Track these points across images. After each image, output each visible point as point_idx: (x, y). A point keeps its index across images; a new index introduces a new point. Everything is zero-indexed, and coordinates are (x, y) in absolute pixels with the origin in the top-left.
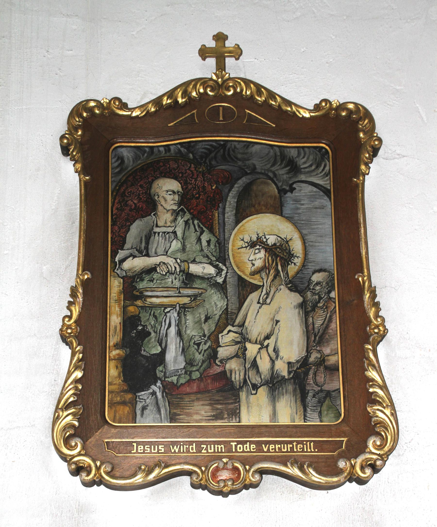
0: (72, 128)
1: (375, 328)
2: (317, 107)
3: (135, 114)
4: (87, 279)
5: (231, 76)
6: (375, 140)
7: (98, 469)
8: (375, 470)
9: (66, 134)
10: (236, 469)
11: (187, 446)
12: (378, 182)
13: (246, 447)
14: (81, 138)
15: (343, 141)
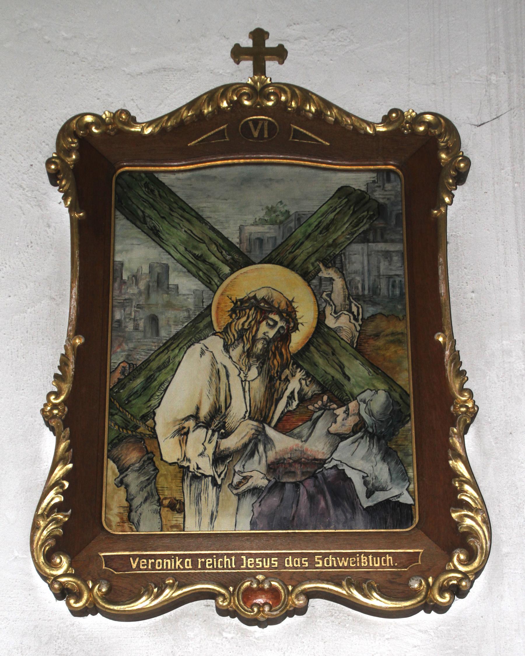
0: (62, 149)
1: (461, 406)
2: (386, 120)
5: (273, 81)
6: (461, 161)
7: (91, 590)
8: (459, 592)
10: (274, 591)
11: (153, 561)
12: (463, 212)
13: (288, 561)
15: (422, 161)
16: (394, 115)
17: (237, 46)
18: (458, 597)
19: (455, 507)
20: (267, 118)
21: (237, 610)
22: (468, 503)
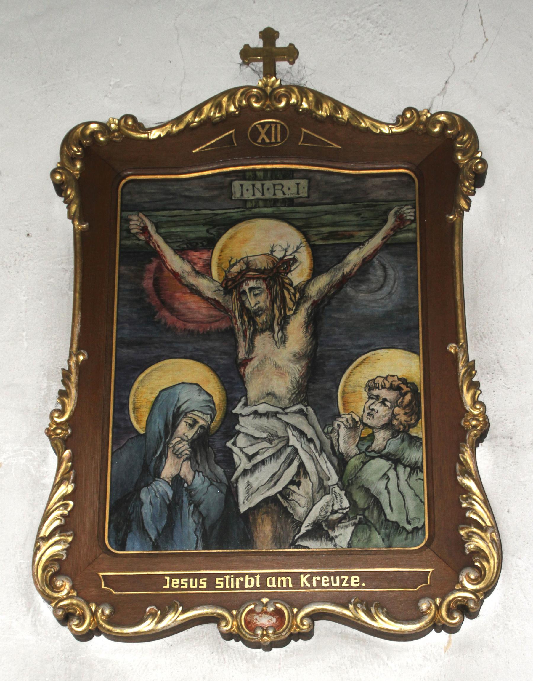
2: (401, 120)
3: (154, 135)
4: (83, 361)
8: (467, 610)
9: (58, 168)
10: (278, 613)
12: (479, 219)
14: (81, 174)
15: (439, 163)
16: (408, 115)
17: (247, 46)
18: (468, 617)
19: (464, 524)
20: (274, 120)
21: (240, 634)
22: (476, 521)
